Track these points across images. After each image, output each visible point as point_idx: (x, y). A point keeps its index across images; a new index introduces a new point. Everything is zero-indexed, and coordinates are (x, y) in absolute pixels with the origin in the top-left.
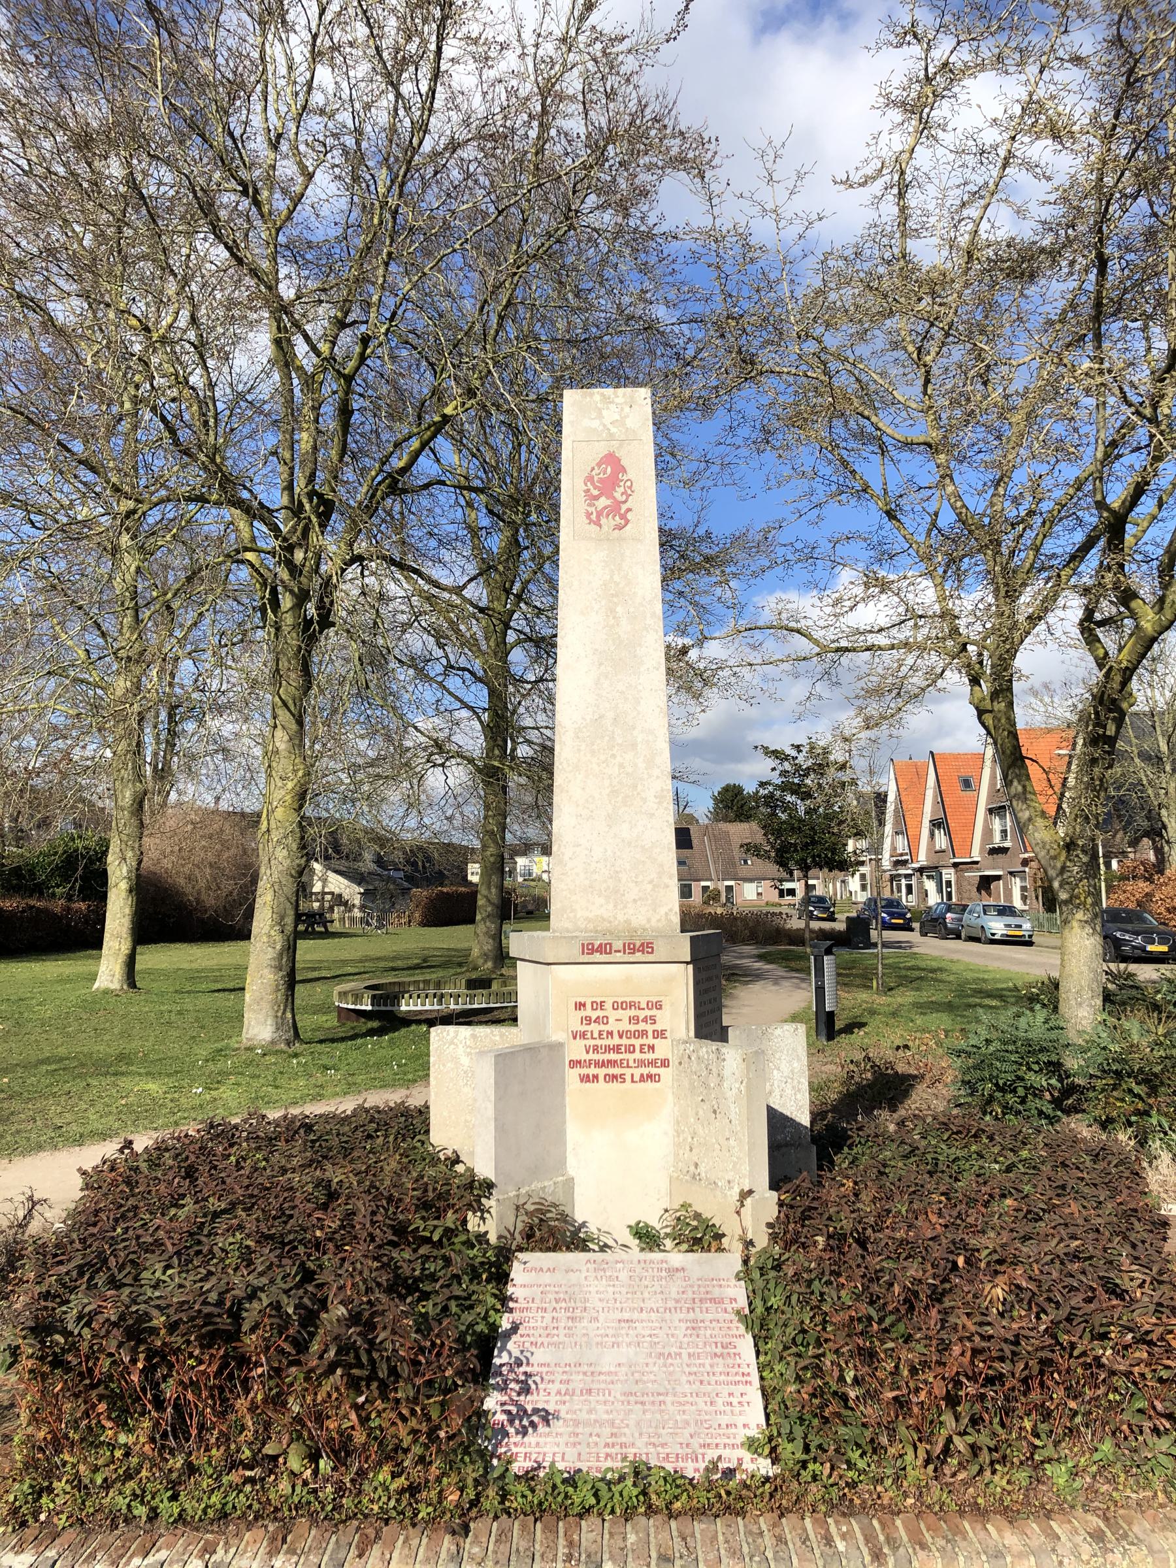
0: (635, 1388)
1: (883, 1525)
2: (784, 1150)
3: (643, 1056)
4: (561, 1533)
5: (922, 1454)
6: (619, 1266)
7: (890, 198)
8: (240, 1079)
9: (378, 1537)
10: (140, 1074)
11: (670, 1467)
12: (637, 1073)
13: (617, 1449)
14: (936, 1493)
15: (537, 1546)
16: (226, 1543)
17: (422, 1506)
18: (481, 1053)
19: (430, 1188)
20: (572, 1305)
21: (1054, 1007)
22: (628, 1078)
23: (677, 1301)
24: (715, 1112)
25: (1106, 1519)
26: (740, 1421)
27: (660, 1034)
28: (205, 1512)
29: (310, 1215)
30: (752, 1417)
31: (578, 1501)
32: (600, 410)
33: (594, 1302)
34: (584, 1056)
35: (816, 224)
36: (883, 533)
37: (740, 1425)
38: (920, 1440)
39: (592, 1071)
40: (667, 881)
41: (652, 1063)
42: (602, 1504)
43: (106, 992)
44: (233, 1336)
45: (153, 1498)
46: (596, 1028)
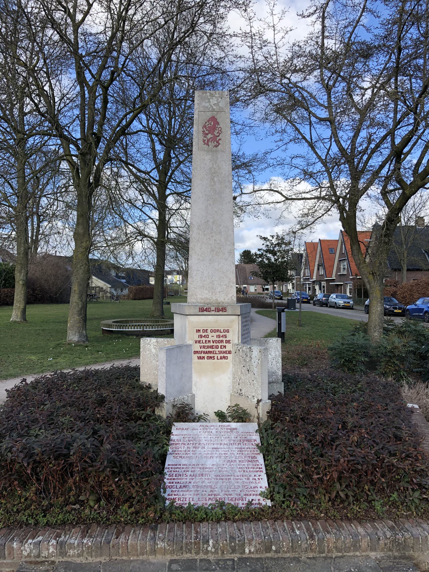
0: (219, 474)
1: (313, 524)
2: (272, 384)
3: (222, 350)
4: (193, 529)
5: (327, 498)
6: (212, 427)
7: (318, 22)
8: (66, 355)
9: (123, 531)
10: (28, 353)
11: (233, 503)
12: (219, 356)
13: (213, 496)
14: (332, 512)
15: (184, 533)
16: (65, 533)
17: (140, 519)
18: (161, 349)
19: (141, 398)
20: (195, 443)
21: (365, 331)
22: (216, 358)
23: (234, 441)
24: (248, 371)
25: (395, 522)
26: (259, 485)
27: (228, 342)
28: (56, 522)
29: (95, 409)
30: (263, 483)
31: (199, 516)
32: (209, 99)
33: (203, 441)
34: (199, 350)
35: (289, 32)
36: (309, 156)
37: (259, 487)
38: (326, 493)
39: (202, 355)
40: (232, 285)
41: (225, 352)
42: (208, 517)
43: (15, 322)
44: (67, 456)
45: (36, 516)
46: (204, 339)
